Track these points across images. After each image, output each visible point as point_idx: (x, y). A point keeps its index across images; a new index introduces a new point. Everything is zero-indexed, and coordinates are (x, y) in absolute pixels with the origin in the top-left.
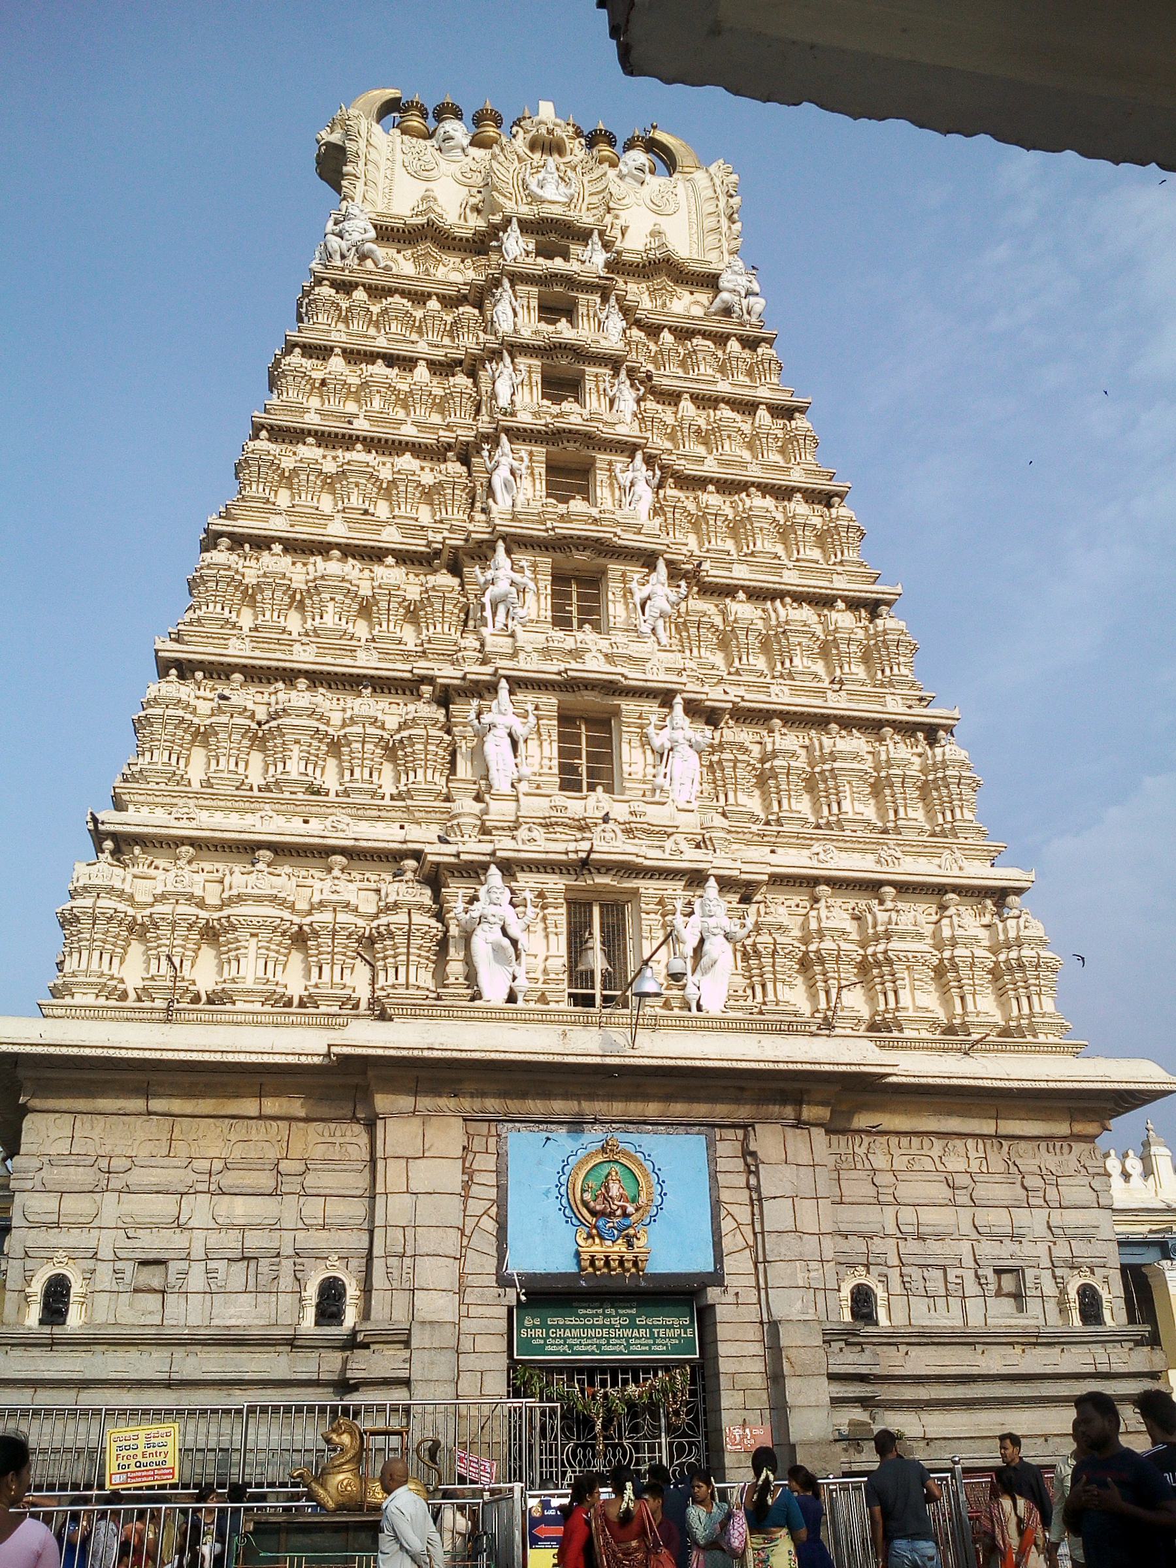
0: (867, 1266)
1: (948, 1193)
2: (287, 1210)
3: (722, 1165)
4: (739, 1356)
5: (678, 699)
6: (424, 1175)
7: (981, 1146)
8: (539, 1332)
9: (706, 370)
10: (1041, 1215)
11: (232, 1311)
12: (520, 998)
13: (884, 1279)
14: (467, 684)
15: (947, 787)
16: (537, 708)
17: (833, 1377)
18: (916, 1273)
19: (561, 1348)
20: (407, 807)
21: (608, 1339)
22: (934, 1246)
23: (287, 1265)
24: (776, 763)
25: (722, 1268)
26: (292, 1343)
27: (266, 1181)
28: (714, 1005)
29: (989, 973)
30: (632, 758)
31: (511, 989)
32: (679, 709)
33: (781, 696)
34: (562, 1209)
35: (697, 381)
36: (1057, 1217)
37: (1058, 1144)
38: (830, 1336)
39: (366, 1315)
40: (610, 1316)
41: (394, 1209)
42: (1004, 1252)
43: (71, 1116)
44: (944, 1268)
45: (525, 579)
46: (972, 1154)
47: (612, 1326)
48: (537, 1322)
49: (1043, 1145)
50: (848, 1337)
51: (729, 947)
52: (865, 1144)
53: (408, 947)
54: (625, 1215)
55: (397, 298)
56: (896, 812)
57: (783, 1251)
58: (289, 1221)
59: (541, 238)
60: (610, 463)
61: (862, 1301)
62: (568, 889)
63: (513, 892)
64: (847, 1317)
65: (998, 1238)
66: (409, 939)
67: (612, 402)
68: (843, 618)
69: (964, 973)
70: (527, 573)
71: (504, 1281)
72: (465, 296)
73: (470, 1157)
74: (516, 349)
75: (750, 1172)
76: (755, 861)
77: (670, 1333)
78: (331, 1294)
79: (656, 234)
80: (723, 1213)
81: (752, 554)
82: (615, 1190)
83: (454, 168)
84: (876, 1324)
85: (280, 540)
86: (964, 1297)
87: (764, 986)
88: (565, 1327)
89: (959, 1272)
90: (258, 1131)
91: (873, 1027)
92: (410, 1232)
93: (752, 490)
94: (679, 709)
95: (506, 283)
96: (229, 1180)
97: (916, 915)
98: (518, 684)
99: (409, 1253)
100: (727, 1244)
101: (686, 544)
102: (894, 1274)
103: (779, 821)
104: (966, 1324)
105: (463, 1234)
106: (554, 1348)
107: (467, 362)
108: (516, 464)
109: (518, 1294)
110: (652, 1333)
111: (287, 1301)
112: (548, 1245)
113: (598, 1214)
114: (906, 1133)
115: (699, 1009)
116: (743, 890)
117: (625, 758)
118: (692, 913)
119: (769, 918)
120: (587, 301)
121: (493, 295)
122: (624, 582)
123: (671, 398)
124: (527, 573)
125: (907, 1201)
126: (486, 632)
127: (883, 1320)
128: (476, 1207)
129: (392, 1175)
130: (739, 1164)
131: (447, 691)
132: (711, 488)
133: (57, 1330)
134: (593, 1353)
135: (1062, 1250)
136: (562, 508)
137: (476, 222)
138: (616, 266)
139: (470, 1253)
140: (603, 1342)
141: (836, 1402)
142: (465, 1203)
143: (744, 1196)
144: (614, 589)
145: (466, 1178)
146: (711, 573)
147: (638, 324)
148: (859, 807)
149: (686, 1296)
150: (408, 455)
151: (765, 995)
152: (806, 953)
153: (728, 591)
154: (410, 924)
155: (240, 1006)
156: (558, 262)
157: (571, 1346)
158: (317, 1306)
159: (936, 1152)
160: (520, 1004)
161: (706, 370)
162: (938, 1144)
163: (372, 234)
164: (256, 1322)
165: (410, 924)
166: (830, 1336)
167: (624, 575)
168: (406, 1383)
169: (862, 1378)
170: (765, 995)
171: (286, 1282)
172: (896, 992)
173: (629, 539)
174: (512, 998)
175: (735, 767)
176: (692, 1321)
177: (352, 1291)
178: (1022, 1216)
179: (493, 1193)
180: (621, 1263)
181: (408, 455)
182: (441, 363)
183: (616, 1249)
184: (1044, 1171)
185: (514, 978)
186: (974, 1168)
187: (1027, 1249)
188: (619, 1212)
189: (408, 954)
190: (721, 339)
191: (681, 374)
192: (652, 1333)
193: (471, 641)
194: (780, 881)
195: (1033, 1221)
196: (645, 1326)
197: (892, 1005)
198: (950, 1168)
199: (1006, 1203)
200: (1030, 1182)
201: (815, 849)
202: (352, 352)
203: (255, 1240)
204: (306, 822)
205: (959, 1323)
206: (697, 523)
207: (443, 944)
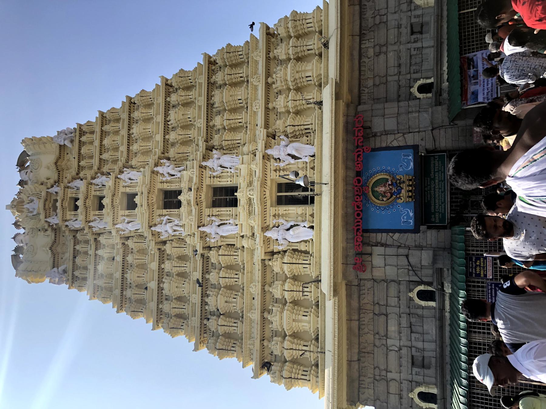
7: (364, 42)
8: (437, 215)
10: (390, 17)
13: (416, 80)
15: (231, 57)
16: (209, 216)
19: (443, 207)
21: (439, 189)
22: (403, 61)
29: (298, 40)
31: (308, 228)
36: (392, 9)
37: (363, 10)
38: (438, 103)
42: (406, 31)
46: (367, 45)
47: (434, 187)
48: (433, 216)
49: (363, 16)
52: (364, 89)
57: (405, 122)
64: (430, 95)
65: (400, 34)
69: (299, 49)
71: (416, 230)
77: (437, 165)
80: (391, 145)
84: (432, 83)
86: (423, 47)
88: (435, 206)
89: (412, 50)
92: (399, 267)
93: (131, 132)
100: (402, 144)
103: (246, 123)
104: (433, 47)
110: (437, 172)
118: (279, 158)
125: (385, 71)
126: (183, 235)
127: (431, 80)
131: (205, 248)
133: (438, 397)
135: (404, 7)
137: (49, 232)
140: (440, 191)
142: (359, 364)
150: (127, 258)
159: (366, 60)
163: (55, 269)
172: (307, 77)
174: (312, 227)
178: (392, 23)
179: (384, 235)
181: (127, 258)
183: (404, 188)
184: (373, 16)
185: (304, 226)
186: (372, 45)
187: (404, 22)
192: (437, 172)
194: (267, 126)
195: (392, 19)
196: (434, 174)
198: (373, 54)
199: (386, 31)
200: (377, 22)
205: (432, 49)
207: (295, 250)
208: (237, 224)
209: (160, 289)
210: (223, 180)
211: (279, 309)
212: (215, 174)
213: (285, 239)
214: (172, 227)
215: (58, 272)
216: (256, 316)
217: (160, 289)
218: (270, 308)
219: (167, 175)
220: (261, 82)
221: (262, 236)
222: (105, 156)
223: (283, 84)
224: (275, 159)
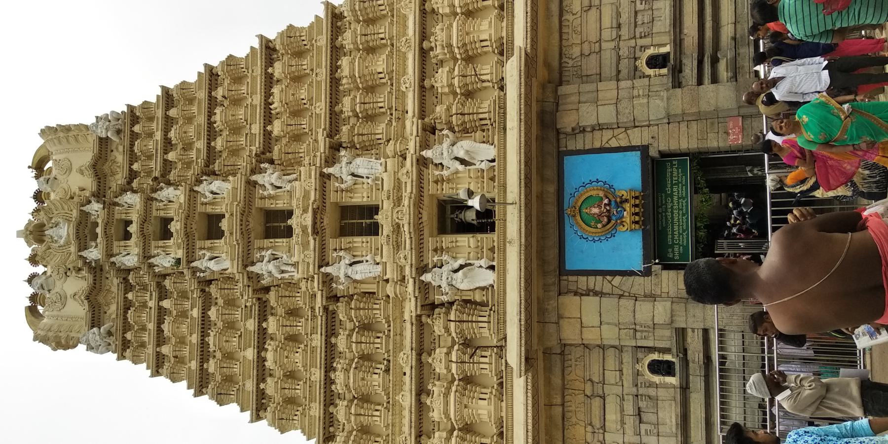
0: (636, 59)
1: (594, 10)
2: (612, 391)
3: (580, 146)
4: (686, 140)
5: (325, 170)
6: (590, 317)
8: (676, 249)
9: (151, 145)
11: (668, 421)
13: (644, 48)
14: (325, 289)
16: (336, 250)
17: (700, 82)
18: (639, 30)
21: (679, 209)
22: (624, 18)
23: (642, 391)
24: (358, 110)
25: (638, 146)
26: (685, 388)
27: (597, 402)
28: (491, 152)
30: (360, 198)
31: (487, 268)
32: (330, 170)
33: (321, 107)
34: (607, 239)
35: (157, 150)
38: (677, 84)
39: (667, 351)
40: (666, 208)
41: (609, 335)
43: (584, 329)
44: (636, 13)
45: (267, 254)
47: (672, 207)
48: (670, 250)
50: (677, 71)
51: (459, 144)
52: (566, 60)
53: (468, 321)
54: (609, 204)
55: (129, 315)
56: (382, 39)
57: (627, 111)
58: (618, 390)
59: (88, 238)
60: (202, 204)
61: (656, 62)
64: (664, 71)
67: (170, 201)
68: (278, 70)
70: (263, 253)
71: (647, 272)
72: (124, 279)
73: (580, 291)
74: (146, 256)
75: (584, 130)
76: (412, 126)
77: (675, 174)
78: (659, 368)
79: (81, 172)
80: (607, 146)
81: (246, 121)
82: (595, 210)
83: (58, 283)
85: (258, 384)
87: (481, 119)
88: (673, 234)
90: (572, 406)
91: (501, 53)
94: (330, 170)
95: (113, 259)
96: (597, 423)
97: (439, 34)
98: (323, 262)
99: (633, 326)
101: (243, 162)
102: (641, 42)
105: (622, 295)
106: (685, 240)
107: (157, 279)
108: (206, 258)
109: (656, 264)
110: (675, 184)
111: (661, 392)
112: (628, 248)
113: (609, 222)
114: (561, 36)
115: (493, 161)
116: (429, 132)
117: (360, 200)
118: (441, 164)
119: (443, 117)
120: (119, 213)
123: (167, 166)
124: (263, 253)
128: (607, 288)
129: (591, 337)
130: (580, 137)
131: (330, 298)
132: (213, 144)
134: (687, 218)
136: (227, 234)
138: (99, 195)
139: (633, 292)
141: (715, 80)
143: (597, 134)
144: (269, 205)
145: (591, 293)
146: (257, 146)
147: (129, 183)
148: (380, 64)
149: (656, 167)
150: (210, 313)
151: (486, 119)
152: (462, 94)
153: (267, 135)
155: (504, 414)
156: (99, 230)
157: (684, 231)
158: (663, 375)
160: (494, 263)
161: (151, 145)
162: (567, 16)
164: (673, 408)
166: (677, 84)
167: (261, 198)
168: (706, 332)
169: (700, 63)
170: (486, 119)
171: (652, 392)
173: (240, 195)
174: (492, 268)
175: (362, 135)
176: (668, 161)
177: (655, 356)
179: (600, 278)
180: (636, 206)
181: (210, 313)
182: (160, 293)
183: (628, 209)
185: (481, 267)
188: (608, 208)
190: (134, 136)
192: (675, 184)
193: (303, 285)
194: (422, 113)
196: (672, 188)
197: (488, 43)
198: (579, 8)
201: (404, 90)
202: (158, 341)
203: (629, 408)
204: (405, 374)
206: (235, 152)
211: (443, 390)
212: (343, 186)
215: (100, 334)
223: (446, 51)
224: (436, 165)
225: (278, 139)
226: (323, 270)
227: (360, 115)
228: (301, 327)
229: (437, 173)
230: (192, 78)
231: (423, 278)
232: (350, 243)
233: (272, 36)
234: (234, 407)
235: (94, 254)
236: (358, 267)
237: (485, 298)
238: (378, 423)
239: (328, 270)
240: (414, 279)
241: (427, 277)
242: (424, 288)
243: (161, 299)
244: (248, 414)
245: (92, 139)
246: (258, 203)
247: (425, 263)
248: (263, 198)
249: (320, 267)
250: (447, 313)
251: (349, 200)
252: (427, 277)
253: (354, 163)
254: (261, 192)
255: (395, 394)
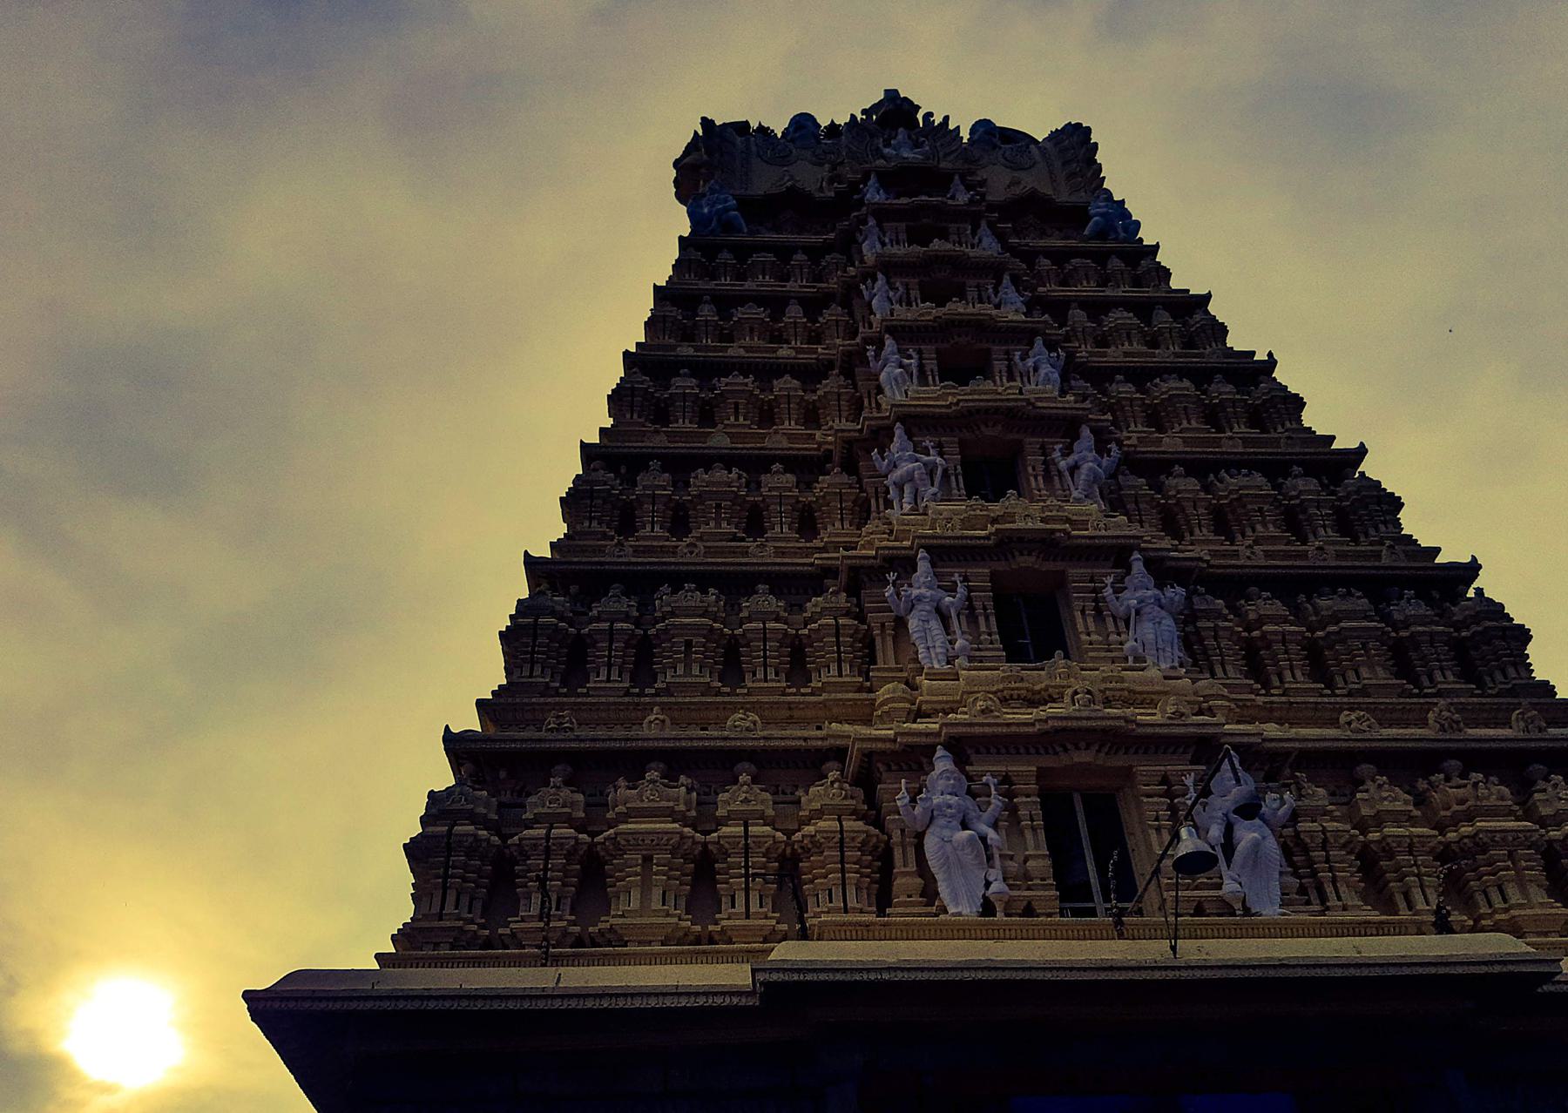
12: (999, 907)
20: (823, 703)
32: (1138, 567)
53: (842, 862)
60: (1007, 353)
62: (1041, 774)
63: (970, 778)
66: (842, 852)
85: (658, 457)
94: (1138, 567)
121: (861, 232)
122: (1169, 794)
150: (787, 377)
154: (841, 831)
156: (936, 244)
165: (841, 831)
167: (1043, 447)
174: (988, 908)
180: (1066, 750)
181: (787, 377)
185: (988, 884)
189: (843, 871)
191: (1376, 916)
207: (885, 858)
208: (945, 667)
209: (633, 763)
210: (1090, 620)
211: (682, 807)
213: (932, 818)
214: (911, 480)
215: (726, 210)
216: (654, 729)
217: (633, 763)
218: (683, 779)
219: (1071, 460)
220: (1441, 736)
221: (930, 740)
222: (1077, 315)
223: (1456, 807)
225: (1159, 488)
226: (922, 553)
227: (1256, 633)
228: (781, 530)
229: (1189, 781)
230: (1235, 342)
231: (940, 752)
232: (985, 608)
233: (1369, 467)
234: (560, 530)
235: (874, 195)
236: (935, 625)
237: (903, 898)
238: (592, 677)
239: (923, 566)
240: (938, 734)
241: (943, 763)
242: (913, 759)
243: (804, 301)
244: (470, 721)
245: (1081, 197)
246: (1031, 443)
247: (973, 757)
248: (1044, 450)
249: (928, 548)
250: (856, 814)
251: (1078, 604)
252: (943, 763)
253: (1163, 613)
254: (1058, 447)
255: (665, 708)
